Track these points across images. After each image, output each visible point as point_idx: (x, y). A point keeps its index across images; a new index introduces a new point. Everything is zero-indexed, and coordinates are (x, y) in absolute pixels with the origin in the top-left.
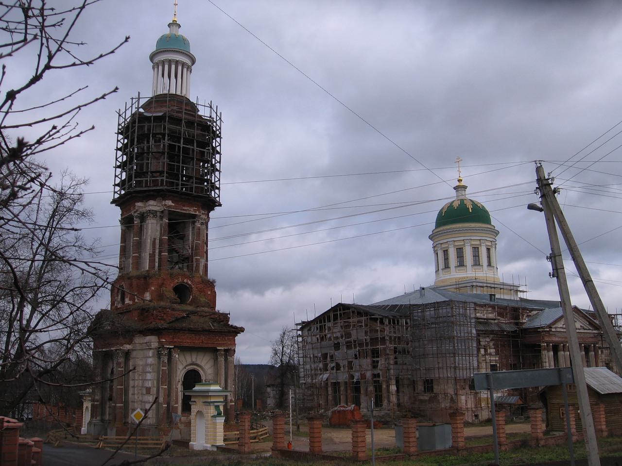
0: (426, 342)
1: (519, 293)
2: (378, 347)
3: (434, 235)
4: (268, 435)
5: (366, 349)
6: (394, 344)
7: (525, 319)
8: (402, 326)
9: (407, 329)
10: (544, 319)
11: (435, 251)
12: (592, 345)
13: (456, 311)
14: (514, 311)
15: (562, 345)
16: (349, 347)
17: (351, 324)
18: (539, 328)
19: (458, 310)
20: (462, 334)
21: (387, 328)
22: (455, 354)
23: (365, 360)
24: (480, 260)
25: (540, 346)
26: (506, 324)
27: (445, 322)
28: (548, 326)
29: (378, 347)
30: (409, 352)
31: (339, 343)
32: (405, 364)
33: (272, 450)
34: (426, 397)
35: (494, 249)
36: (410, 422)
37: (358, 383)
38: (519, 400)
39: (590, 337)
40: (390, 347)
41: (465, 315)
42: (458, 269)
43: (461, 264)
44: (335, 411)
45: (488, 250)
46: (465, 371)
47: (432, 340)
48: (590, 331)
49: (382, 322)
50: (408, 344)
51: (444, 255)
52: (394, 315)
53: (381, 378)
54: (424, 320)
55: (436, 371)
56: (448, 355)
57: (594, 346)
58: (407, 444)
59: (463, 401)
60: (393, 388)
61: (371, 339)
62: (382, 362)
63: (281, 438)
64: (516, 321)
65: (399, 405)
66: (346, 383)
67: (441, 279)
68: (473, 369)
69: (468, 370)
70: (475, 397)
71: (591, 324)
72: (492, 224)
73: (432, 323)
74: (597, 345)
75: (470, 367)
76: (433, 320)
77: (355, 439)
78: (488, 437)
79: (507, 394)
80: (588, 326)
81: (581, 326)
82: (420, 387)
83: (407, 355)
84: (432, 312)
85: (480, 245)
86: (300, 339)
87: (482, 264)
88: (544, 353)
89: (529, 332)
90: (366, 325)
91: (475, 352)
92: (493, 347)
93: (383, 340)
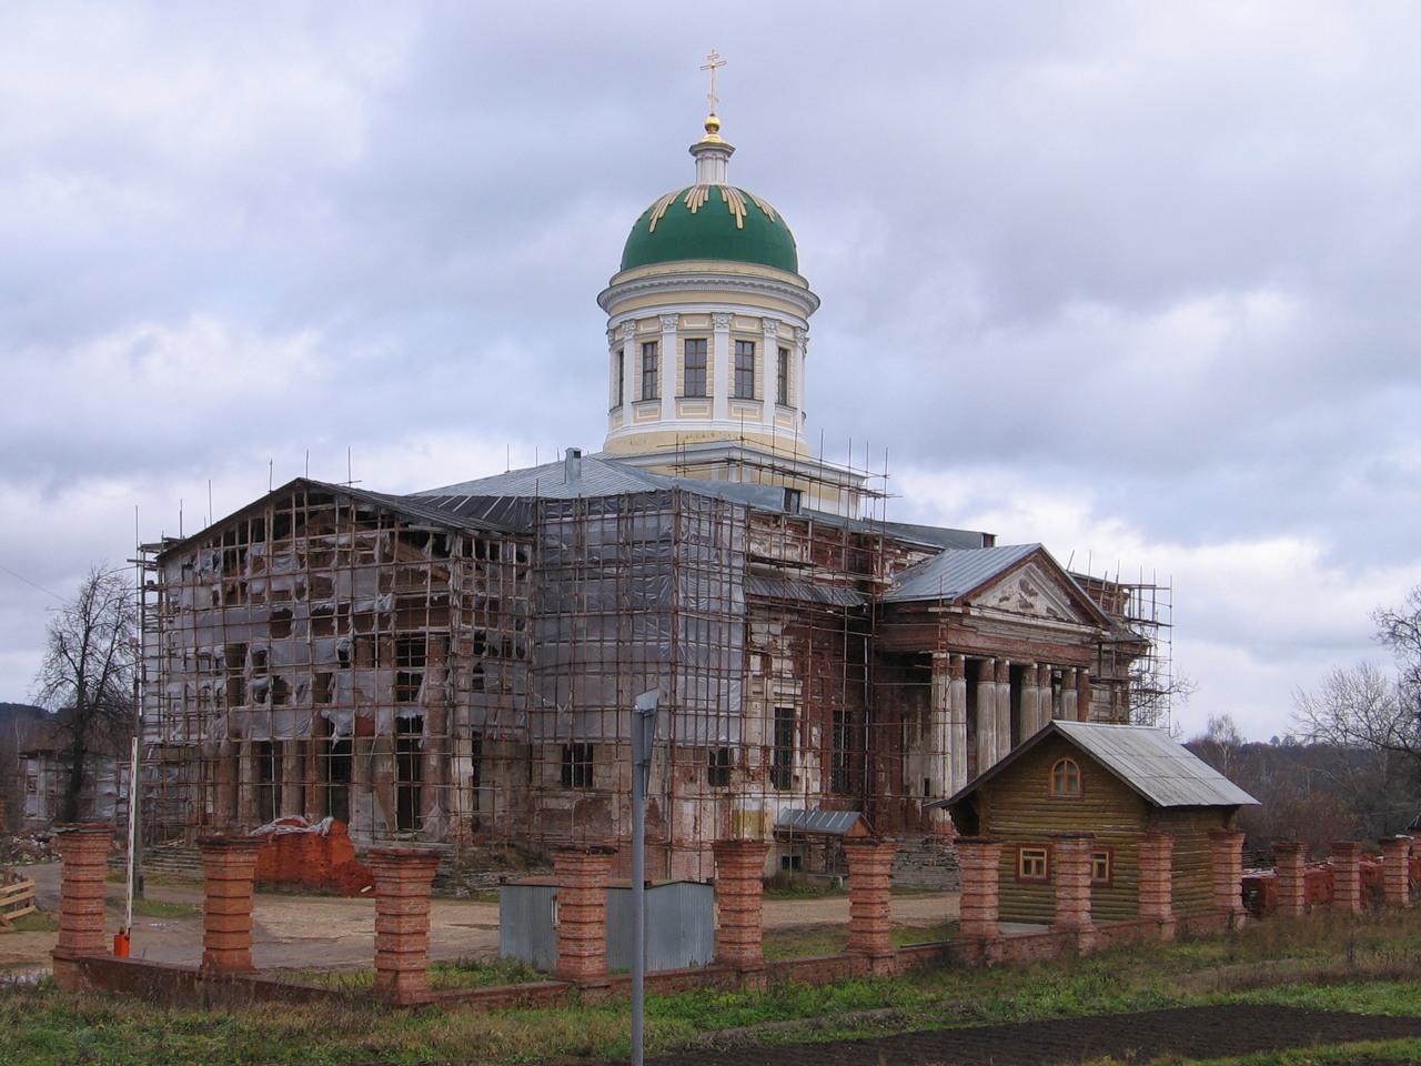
0: (581, 623)
1: (863, 499)
2: (421, 629)
3: (614, 292)
4: (32, 908)
5: (380, 636)
6: (477, 624)
7: (888, 575)
8: (507, 566)
9: (521, 576)
10: (944, 580)
11: (613, 343)
12: (1074, 670)
13: (689, 527)
14: (859, 546)
15: (993, 661)
16: (321, 623)
17: (336, 549)
18: (935, 603)
19: (694, 524)
20: (703, 605)
21: (456, 570)
22: (674, 664)
23: (373, 673)
24: (757, 384)
25: (928, 659)
26: (834, 587)
27: (649, 559)
28: (962, 598)
29: (421, 629)
30: (524, 652)
31: (287, 614)
32: (509, 691)
33: (55, 958)
34: (566, 802)
35: (800, 353)
36: (586, 867)
37: (344, 746)
38: (858, 823)
39: (1071, 645)
40: (464, 633)
41: (715, 543)
42: (683, 404)
43: (695, 389)
44: (266, 835)
45: (783, 353)
46: (712, 721)
47: (603, 616)
48: (1074, 627)
49: (440, 550)
50: (520, 628)
51: (645, 357)
52: (483, 527)
53: (426, 732)
54: (579, 549)
55: (610, 717)
56: (651, 668)
57: (1078, 673)
58: (572, 948)
59: (689, 821)
60: (463, 767)
61: (400, 603)
62: (430, 676)
63: (92, 914)
64: (861, 577)
65: (476, 825)
66: (302, 745)
67: (626, 433)
68: (728, 718)
69: (712, 721)
70: (725, 808)
71: (1077, 604)
72: (800, 272)
73: (608, 563)
74: (1087, 671)
75: (718, 711)
76: (611, 553)
77: (389, 925)
78: (783, 934)
79: (818, 804)
80: (1068, 611)
81: (1049, 610)
82: (551, 770)
83: (515, 661)
84: (611, 527)
85: (761, 336)
86: (152, 597)
87: (762, 394)
88: (941, 681)
89: (901, 614)
90: (387, 558)
91: (737, 665)
92: (788, 653)
93: (441, 609)
